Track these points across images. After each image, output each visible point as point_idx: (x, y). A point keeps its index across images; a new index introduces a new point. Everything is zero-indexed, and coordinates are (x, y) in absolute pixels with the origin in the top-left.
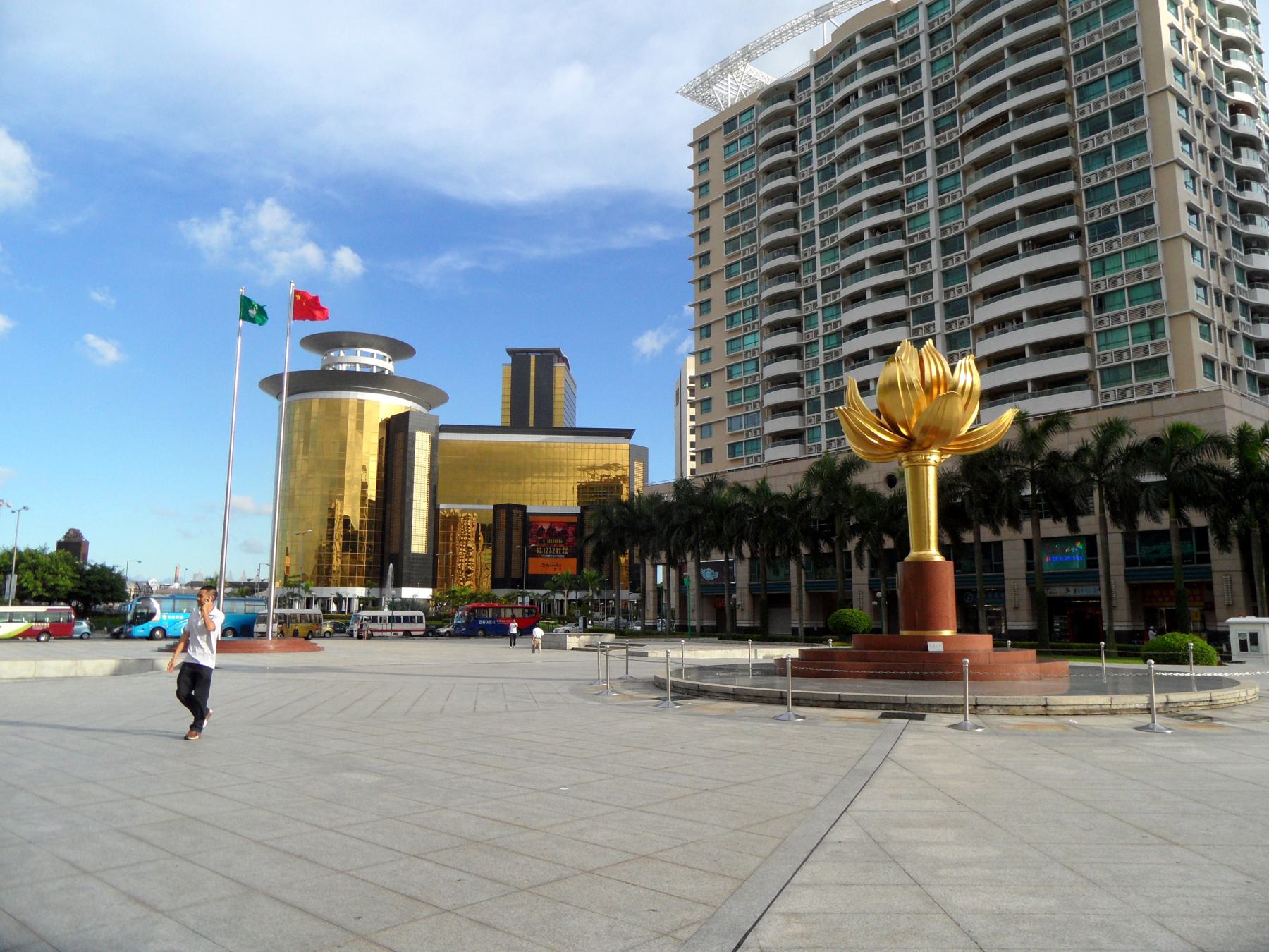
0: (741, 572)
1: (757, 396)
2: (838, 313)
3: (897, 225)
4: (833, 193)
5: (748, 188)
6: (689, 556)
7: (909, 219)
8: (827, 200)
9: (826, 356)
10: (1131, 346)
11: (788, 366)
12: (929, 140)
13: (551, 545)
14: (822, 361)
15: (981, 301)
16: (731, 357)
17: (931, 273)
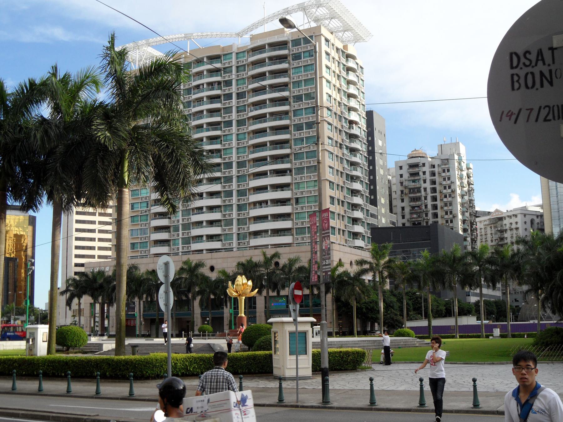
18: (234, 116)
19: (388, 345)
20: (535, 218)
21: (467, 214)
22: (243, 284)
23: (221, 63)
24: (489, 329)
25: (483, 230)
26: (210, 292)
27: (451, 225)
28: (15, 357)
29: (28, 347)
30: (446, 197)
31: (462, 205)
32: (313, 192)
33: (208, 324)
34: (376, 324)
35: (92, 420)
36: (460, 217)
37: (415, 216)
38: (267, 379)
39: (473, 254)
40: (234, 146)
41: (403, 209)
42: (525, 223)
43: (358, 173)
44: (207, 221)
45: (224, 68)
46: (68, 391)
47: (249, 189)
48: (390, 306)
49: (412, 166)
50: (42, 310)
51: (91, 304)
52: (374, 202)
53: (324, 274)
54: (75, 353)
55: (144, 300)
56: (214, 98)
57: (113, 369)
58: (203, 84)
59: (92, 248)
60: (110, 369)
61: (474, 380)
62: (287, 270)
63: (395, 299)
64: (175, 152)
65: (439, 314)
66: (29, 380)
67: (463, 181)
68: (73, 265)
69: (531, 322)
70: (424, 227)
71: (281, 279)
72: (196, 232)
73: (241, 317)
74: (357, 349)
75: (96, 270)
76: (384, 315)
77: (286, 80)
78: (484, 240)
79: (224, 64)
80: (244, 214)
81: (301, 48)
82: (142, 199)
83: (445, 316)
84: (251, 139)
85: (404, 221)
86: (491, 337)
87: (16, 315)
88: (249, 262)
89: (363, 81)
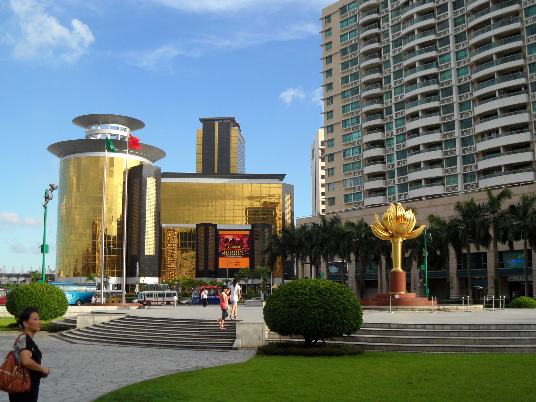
0: (351, 268)
1: (360, 168)
2: (404, 123)
3: (435, 76)
4: (400, 55)
5: (354, 47)
6: (322, 260)
7: (441, 73)
8: (397, 58)
9: (398, 147)
11: (377, 152)
12: (451, 30)
13: (233, 250)
14: (395, 150)
15: (481, 157)
16: (345, 145)
17: (449, 36)
72: (413, 176)
82: (354, 144)
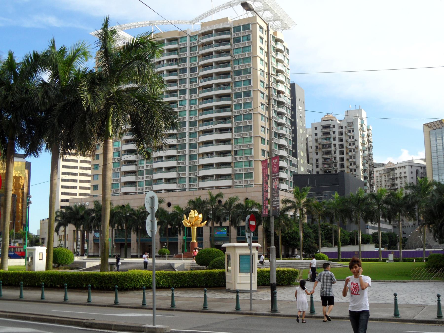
1: (118, 166)
10: (243, 168)
18: (188, 86)
19: (314, 266)
20: (419, 169)
21: (367, 165)
22: (195, 217)
23: (178, 44)
24: (385, 255)
25: (379, 178)
26: (167, 223)
27: (354, 173)
28: (20, 271)
29: (27, 264)
30: (350, 151)
31: (363, 158)
32: (248, 146)
33: (166, 248)
34: (296, 250)
35: (90, 323)
36: (362, 167)
37: (326, 166)
38: (221, 292)
39: (373, 196)
40: (186, 111)
41: (317, 160)
42: (412, 172)
43: (283, 131)
44: (165, 168)
45: (180, 48)
46: (65, 299)
47: (199, 143)
48: (307, 235)
49: (324, 127)
50: (35, 236)
51: (74, 231)
52: (295, 155)
53: (274, 208)
54: (64, 269)
55: (116, 228)
56: (172, 72)
57: (99, 282)
58: (164, 61)
59: (75, 188)
60: (97, 282)
61: (395, 295)
62: (228, 206)
63: (311, 231)
64: (149, 109)
65: (345, 243)
66: (32, 290)
67: (364, 139)
68: (60, 200)
69: (417, 250)
70: (334, 174)
71: (223, 214)
72: (156, 176)
73: (193, 243)
74: (291, 269)
75: (79, 204)
76: (303, 243)
77: (228, 58)
78: (379, 186)
79: (181, 45)
80: (195, 163)
81: (241, 33)
83: (349, 244)
84: (201, 104)
85: (318, 170)
86: (387, 261)
87: (16, 239)
88: (198, 200)
89: (288, 60)
